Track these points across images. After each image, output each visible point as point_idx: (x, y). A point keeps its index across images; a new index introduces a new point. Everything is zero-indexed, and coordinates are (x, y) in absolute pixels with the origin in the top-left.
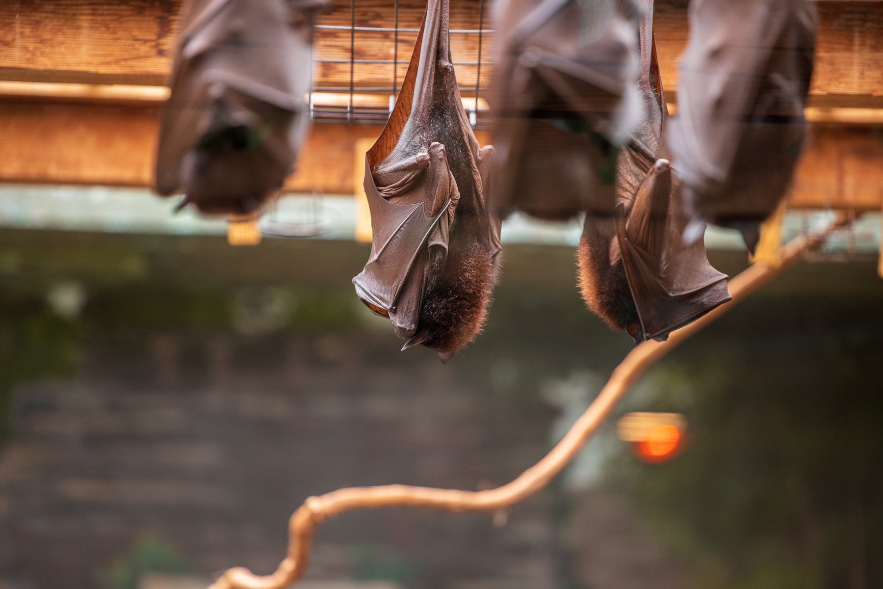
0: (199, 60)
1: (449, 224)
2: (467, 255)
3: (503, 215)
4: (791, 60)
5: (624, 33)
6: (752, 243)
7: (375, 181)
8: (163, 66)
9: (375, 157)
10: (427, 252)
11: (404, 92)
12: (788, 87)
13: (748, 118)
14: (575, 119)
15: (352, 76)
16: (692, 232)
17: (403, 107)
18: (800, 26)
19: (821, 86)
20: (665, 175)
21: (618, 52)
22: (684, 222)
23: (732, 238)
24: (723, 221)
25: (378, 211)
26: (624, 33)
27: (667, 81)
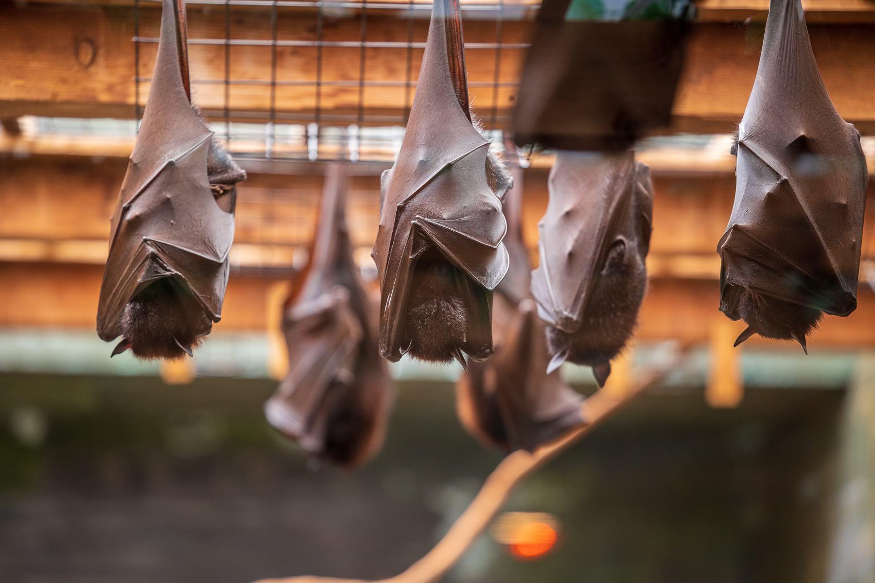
0: (137, 223)
1: (455, 89)
2: (444, 185)
3: (395, 357)
4: (631, 224)
5: (494, 200)
6: (603, 376)
7: (288, 325)
8: (107, 229)
9: (288, 303)
10: (333, 384)
11: (311, 248)
12: (631, 244)
13: (598, 266)
14: (455, 271)
15: (307, 131)
16: (552, 366)
17: (308, 266)
18: (638, 193)
19: (659, 239)
20: (530, 320)
21: (490, 214)
22: (548, 359)
23: (585, 372)
24: (577, 357)
25: (292, 349)
26: (494, 200)
27: (532, 236)
